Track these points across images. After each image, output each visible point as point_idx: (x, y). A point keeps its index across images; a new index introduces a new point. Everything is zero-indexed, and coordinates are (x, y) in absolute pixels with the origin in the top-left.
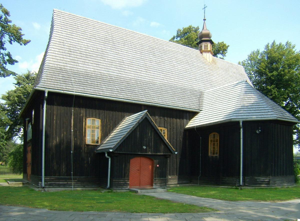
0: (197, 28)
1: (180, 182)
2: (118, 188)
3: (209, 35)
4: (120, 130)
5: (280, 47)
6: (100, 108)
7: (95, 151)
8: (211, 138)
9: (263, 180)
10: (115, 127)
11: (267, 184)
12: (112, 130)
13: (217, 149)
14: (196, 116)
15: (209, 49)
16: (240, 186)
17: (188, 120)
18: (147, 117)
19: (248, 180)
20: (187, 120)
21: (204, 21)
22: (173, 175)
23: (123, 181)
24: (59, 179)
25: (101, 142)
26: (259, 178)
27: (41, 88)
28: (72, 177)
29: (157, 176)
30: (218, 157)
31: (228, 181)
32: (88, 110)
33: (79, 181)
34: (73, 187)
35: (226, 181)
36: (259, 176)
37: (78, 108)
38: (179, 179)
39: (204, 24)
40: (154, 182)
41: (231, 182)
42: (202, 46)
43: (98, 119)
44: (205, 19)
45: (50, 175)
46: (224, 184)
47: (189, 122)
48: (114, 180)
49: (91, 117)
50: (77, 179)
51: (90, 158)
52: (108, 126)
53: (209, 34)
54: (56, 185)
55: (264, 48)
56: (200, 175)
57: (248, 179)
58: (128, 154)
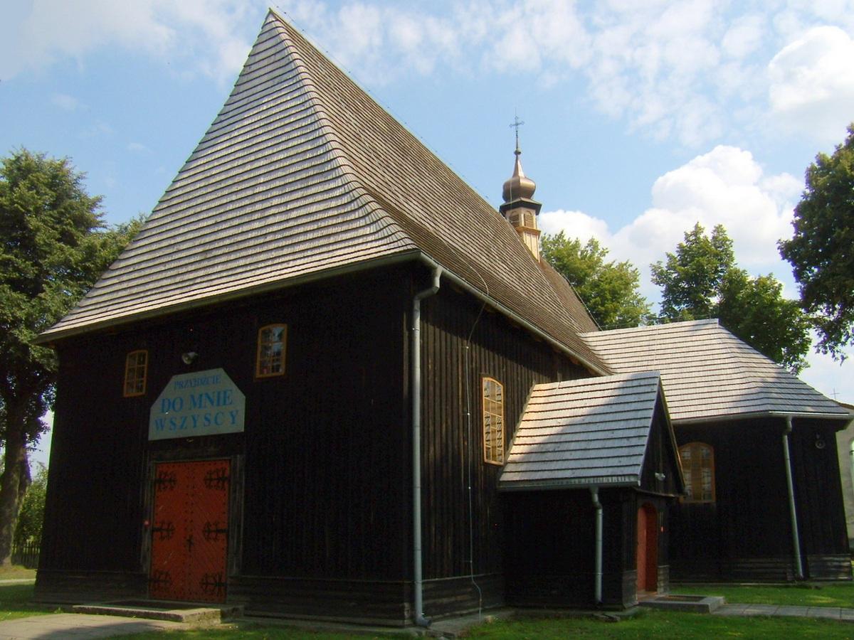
4: (554, 431)
13: (708, 480)
16: (799, 579)
28: (472, 576)
36: (828, 553)
42: (518, 215)
44: (520, 150)
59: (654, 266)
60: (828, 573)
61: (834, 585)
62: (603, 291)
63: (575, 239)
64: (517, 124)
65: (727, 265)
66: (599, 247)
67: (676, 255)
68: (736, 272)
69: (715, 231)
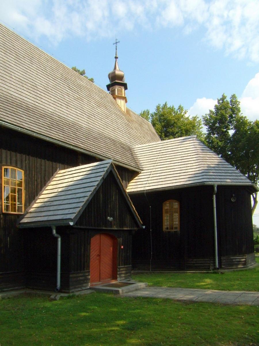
0: (82, 72)
5: (172, 109)
7: (18, 226)
8: (166, 206)
9: (239, 260)
10: (45, 186)
12: (41, 191)
14: (136, 178)
17: (127, 182)
18: (112, 170)
19: (224, 261)
20: (126, 181)
21: (115, 59)
25: (25, 210)
30: (179, 232)
31: (197, 263)
35: (194, 264)
36: (235, 255)
39: (116, 63)
41: (202, 265)
42: (115, 90)
43: (20, 169)
44: (117, 56)
46: (190, 268)
47: (128, 185)
49: (10, 164)
51: (8, 238)
52: (35, 183)
53: (123, 77)
55: (155, 109)
56: (151, 258)
58: (88, 229)
59: (203, 116)
60: (232, 265)
61: (234, 271)
62: (182, 130)
63: (164, 104)
64: (116, 43)
65: (236, 114)
66: (184, 110)
67: (214, 110)
68: (241, 118)
69: (231, 97)
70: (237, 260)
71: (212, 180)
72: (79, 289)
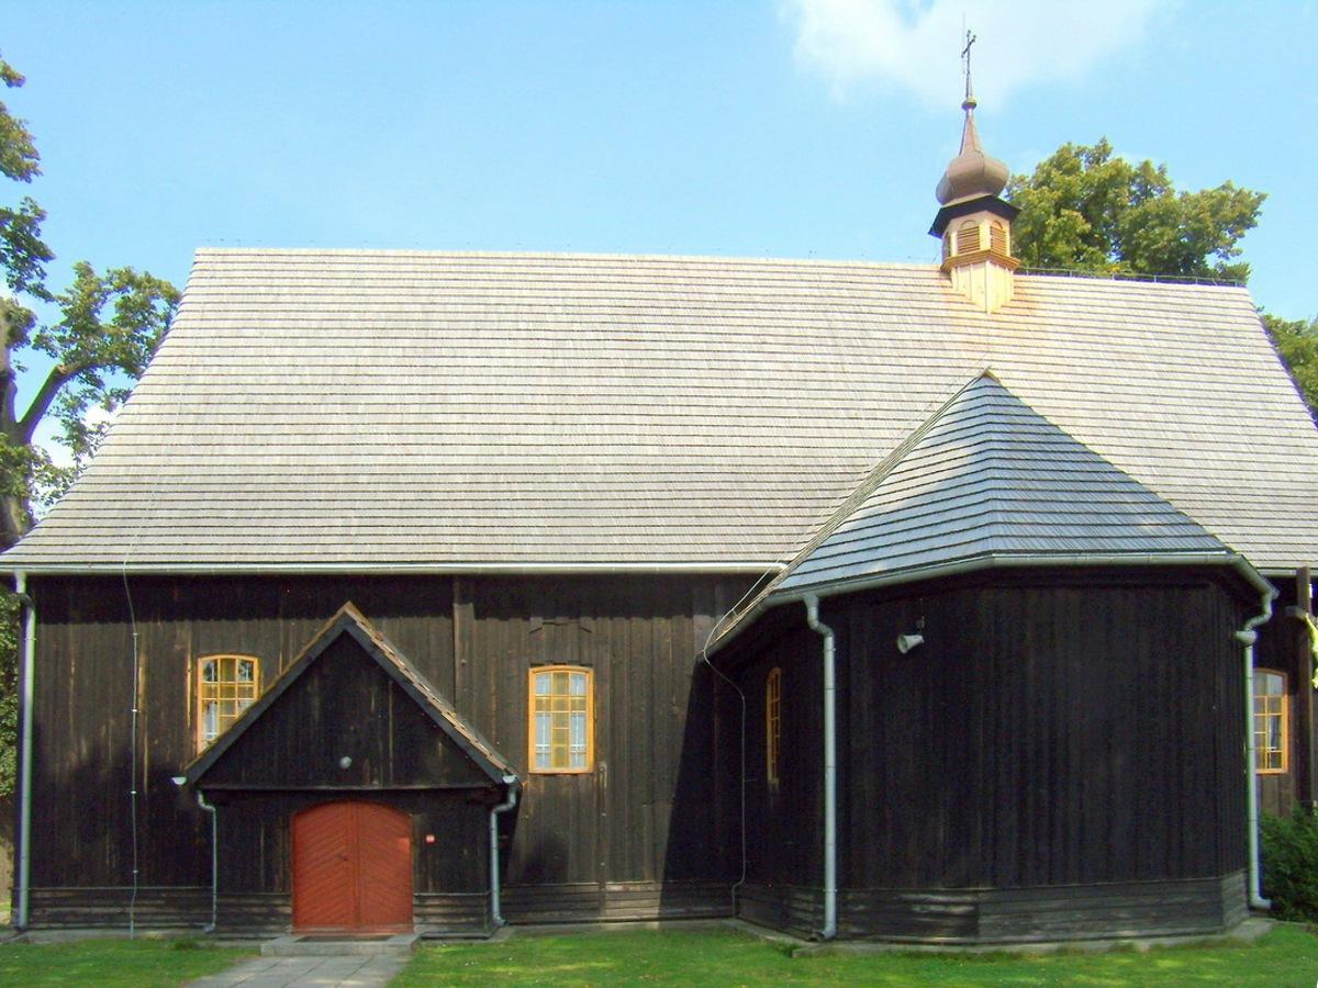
1: (681, 910)
2: (240, 932)
3: (986, 170)
6: (233, 613)
9: (941, 909)
11: (961, 931)
15: (985, 245)
21: (964, 112)
22: (633, 876)
23: (260, 902)
24: (89, 898)
26: (922, 896)
27: (86, 567)
28: (135, 888)
29: (430, 884)
32: (200, 623)
33: (170, 902)
34: (132, 929)
37: (164, 622)
38: (667, 897)
40: (417, 910)
44: (974, 98)
45: (55, 881)
48: (798, 896)
50: (164, 895)
54: (80, 919)
57: (862, 902)
70: (933, 908)
71: (1069, 531)
72: (250, 935)
